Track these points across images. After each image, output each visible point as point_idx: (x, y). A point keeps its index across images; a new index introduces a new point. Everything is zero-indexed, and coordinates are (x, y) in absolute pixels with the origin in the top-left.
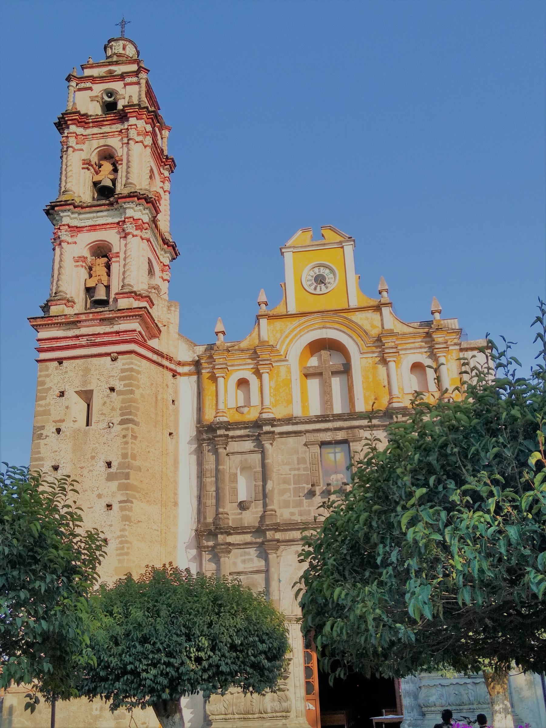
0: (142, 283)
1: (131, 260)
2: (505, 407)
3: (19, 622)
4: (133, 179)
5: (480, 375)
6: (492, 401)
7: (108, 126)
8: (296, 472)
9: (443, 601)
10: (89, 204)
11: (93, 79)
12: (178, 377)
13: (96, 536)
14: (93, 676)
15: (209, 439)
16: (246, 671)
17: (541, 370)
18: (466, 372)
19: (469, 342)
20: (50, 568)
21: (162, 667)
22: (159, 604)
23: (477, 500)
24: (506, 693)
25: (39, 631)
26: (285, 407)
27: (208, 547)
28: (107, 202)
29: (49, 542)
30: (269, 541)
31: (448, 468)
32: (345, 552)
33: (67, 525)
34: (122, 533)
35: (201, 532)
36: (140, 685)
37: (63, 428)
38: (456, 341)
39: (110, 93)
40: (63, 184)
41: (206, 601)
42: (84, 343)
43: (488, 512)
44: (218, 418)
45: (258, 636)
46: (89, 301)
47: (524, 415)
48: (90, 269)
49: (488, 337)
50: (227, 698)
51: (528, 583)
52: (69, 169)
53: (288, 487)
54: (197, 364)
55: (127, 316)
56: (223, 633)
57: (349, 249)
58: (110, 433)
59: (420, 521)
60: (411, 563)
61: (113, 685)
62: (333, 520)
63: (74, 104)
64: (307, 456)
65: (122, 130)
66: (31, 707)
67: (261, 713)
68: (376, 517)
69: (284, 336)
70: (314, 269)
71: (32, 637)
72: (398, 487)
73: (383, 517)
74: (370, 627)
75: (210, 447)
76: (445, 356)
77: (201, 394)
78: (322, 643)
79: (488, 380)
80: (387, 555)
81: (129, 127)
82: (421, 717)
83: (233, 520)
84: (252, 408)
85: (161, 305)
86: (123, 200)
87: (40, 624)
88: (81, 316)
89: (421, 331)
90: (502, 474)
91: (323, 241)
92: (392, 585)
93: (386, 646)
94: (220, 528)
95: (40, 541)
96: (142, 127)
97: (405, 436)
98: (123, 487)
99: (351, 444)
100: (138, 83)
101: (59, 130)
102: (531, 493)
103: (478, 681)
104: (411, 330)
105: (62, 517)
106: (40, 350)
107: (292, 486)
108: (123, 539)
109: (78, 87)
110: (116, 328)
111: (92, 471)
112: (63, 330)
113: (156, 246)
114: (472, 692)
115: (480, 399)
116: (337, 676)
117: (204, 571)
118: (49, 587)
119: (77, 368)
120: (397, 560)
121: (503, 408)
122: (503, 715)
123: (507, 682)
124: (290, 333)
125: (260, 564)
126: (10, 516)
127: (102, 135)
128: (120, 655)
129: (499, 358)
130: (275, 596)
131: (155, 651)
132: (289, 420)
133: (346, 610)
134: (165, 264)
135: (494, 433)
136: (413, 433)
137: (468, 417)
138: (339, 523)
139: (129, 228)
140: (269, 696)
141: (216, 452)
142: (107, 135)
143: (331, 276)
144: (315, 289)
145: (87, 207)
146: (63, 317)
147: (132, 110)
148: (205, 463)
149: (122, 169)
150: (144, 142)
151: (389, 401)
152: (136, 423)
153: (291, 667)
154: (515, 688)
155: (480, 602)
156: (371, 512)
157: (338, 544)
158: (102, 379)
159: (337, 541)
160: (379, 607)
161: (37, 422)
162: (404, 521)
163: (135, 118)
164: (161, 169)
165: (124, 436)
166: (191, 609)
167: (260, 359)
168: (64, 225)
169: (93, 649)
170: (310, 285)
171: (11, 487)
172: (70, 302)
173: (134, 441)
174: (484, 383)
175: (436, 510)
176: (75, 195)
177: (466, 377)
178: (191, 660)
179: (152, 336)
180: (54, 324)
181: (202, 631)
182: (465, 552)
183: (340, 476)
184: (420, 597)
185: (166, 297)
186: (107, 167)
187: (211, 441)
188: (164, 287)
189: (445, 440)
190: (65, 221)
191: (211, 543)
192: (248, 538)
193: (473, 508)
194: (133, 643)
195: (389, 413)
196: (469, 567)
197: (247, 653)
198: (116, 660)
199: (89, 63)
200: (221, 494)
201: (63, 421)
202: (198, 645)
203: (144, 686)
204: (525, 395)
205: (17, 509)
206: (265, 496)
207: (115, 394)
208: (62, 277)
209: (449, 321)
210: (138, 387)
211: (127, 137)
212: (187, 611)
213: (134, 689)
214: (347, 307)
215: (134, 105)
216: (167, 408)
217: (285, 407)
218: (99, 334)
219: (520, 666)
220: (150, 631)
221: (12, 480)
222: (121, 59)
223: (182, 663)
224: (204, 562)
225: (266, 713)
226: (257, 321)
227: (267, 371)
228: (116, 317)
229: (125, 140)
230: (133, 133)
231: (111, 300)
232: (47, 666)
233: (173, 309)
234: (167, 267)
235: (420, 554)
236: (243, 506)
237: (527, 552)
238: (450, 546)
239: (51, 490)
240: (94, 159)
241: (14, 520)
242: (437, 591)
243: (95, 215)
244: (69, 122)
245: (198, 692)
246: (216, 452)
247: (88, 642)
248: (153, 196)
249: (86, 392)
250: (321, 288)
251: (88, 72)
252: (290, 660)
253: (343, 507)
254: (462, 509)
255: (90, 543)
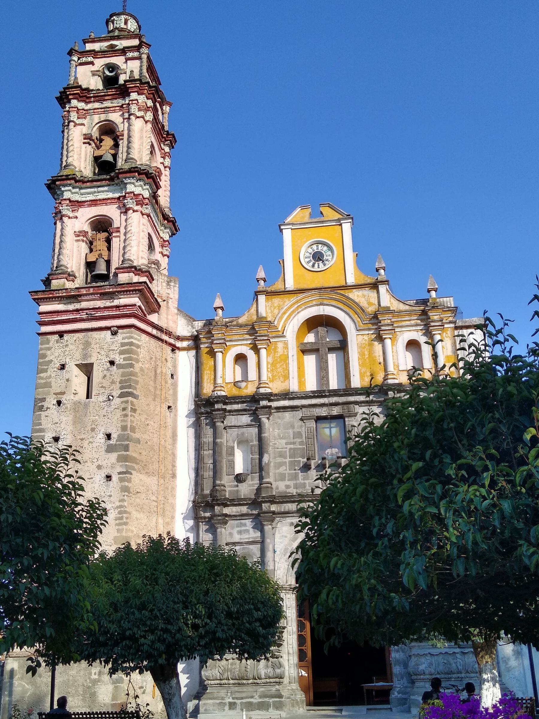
0: (142, 258)
1: (132, 235)
2: (502, 383)
3: (22, 588)
4: (135, 154)
5: (478, 353)
6: (489, 377)
7: (110, 101)
8: (292, 446)
9: (437, 572)
10: (90, 179)
11: (95, 54)
12: (177, 351)
13: (97, 506)
14: (92, 642)
15: (207, 413)
16: (241, 637)
17: (537, 348)
18: (463, 349)
19: (464, 320)
20: (52, 535)
21: (159, 633)
22: (157, 572)
23: (472, 475)
24: (494, 663)
25: (41, 596)
26: (282, 382)
27: (205, 518)
28: (108, 177)
29: (51, 510)
30: (265, 513)
31: (444, 443)
32: (341, 523)
33: (70, 494)
34: (121, 503)
35: (198, 503)
36: (138, 650)
37: (63, 400)
38: (451, 319)
39: (112, 67)
40: (65, 158)
41: (202, 570)
42: (85, 317)
43: (483, 486)
44: (216, 392)
45: (253, 604)
46: (89, 276)
47: (520, 391)
48: (91, 243)
49: (486, 315)
50: (222, 664)
51: (520, 556)
52: (70, 144)
53: (284, 460)
54: (196, 339)
55: (127, 291)
56: (219, 602)
57: (347, 227)
58: (110, 405)
59: (415, 494)
60: (407, 535)
61: (112, 650)
62: (330, 492)
63: (76, 78)
64: (303, 430)
65: (123, 105)
66: (32, 670)
67: (255, 679)
68: (373, 490)
69: (282, 312)
70: (312, 246)
71: (35, 602)
72: (395, 460)
73: (379, 490)
74: (366, 597)
75: (208, 421)
76: (440, 334)
77: (200, 368)
78: (318, 611)
79: (485, 357)
80: (383, 526)
81: (130, 102)
82: (410, 685)
83: (230, 491)
84: (250, 383)
85: (161, 280)
86: (124, 175)
87: (43, 590)
88: (82, 290)
89: (417, 308)
90: (497, 449)
91: (322, 219)
92: (387, 556)
93: (380, 614)
94: (217, 500)
95: (43, 509)
96: (143, 102)
97: (402, 411)
98: (122, 459)
99: (346, 419)
100: (139, 58)
101: (61, 104)
102: (526, 468)
103: (466, 650)
104: (407, 308)
105: (64, 486)
106: (42, 324)
107: (288, 460)
108: (123, 509)
109: (79, 61)
110: (116, 302)
111: (92, 443)
112: (65, 304)
113: (156, 221)
114: (461, 661)
115: (476, 375)
116: (332, 644)
117: (201, 541)
118: (51, 554)
119: (77, 341)
120: (393, 531)
121: (499, 384)
122: (491, 684)
123: (495, 652)
124: (287, 310)
125: (256, 535)
126: (14, 484)
127: (103, 110)
128: (119, 622)
129: (496, 335)
130: (270, 566)
131: (153, 618)
132: (286, 395)
133: (342, 579)
134: (165, 239)
135: (490, 409)
136: (410, 408)
137: (466, 394)
138: (336, 495)
139: (130, 203)
140: (263, 662)
141: (213, 426)
142: (108, 109)
143: (329, 253)
144: (313, 266)
145: (88, 181)
146: (64, 291)
147: (133, 85)
148: (202, 436)
149: (123, 144)
150: (145, 118)
151: (385, 377)
152: (135, 397)
153: (285, 635)
154: (502, 658)
155: (474, 573)
156: (367, 485)
157: (334, 515)
158: (103, 353)
159: (333, 512)
160: (374, 577)
161: (38, 394)
162: (400, 494)
163: (136, 93)
164: (162, 145)
165: (124, 409)
166: (188, 577)
167: (257, 335)
168: (65, 200)
169: (93, 614)
170: (308, 262)
171: (14, 456)
172: (71, 276)
173: (134, 414)
174: (481, 359)
175: (432, 483)
176: (77, 170)
177: (461, 354)
178: (188, 627)
179: (152, 311)
180: (55, 297)
181: (199, 599)
182: (459, 525)
183: (335, 450)
184: (415, 567)
185: (165, 272)
186: (108, 142)
187: (209, 415)
188: (164, 262)
189: (442, 415)
190: (67, 195)
191: (208, 515)
192: (244, 509)
193: (468, 482)
194: (132, 610)
195: (383, 389)
196: (463, 539)
197: (242, 621)
198: (115, 626)
199: (91, 37)
200: (218, 467)
201: (63, 393)
202: (195, 612)
203: (142, 651)
204: (521, 372)
205: (20, 478)
206: (261, 469)
207: (115, 367)
208: (64, 251)
209: (445, 299)
210: (137, 361)
211: (129, 112)
212: (185, 579)
213: (132, 654)
214: (344, 284)
215: (136, 80)
216: (166, 383)
217: (282, 382)
218: (99, 308)
219: (509, 636)
220: (148, 598)
221: (15, 450)
222: (123, 33)
223: (180, 630)
224: (201, 532)
225: (260, 678)
226: (256, 297)
227: (265, 346)
228: (116, 291)
229: (126, 115)
230: (134, 108)
231: (111, 275)
232: (49, 631)
233: (172, 284)
234: (167, 243)
235: (415, 527)
236: (239, 479)
237: (521, 525)
238: (444, 519)
239: (53, 460)
240: (95, 134)
241: (17, 489)
242: (431, 562)
243: (96, 189)
244: (71, 97)
245: (195, 658)
246: (213, 426)
247: (89, 608)
248: (153, 172)
249: (86, 365)
250: (319, 265)
251: (89, 47)
252: (284, 628)
253: (340, 479)
254: (457, 482)
255: (92, 512)
